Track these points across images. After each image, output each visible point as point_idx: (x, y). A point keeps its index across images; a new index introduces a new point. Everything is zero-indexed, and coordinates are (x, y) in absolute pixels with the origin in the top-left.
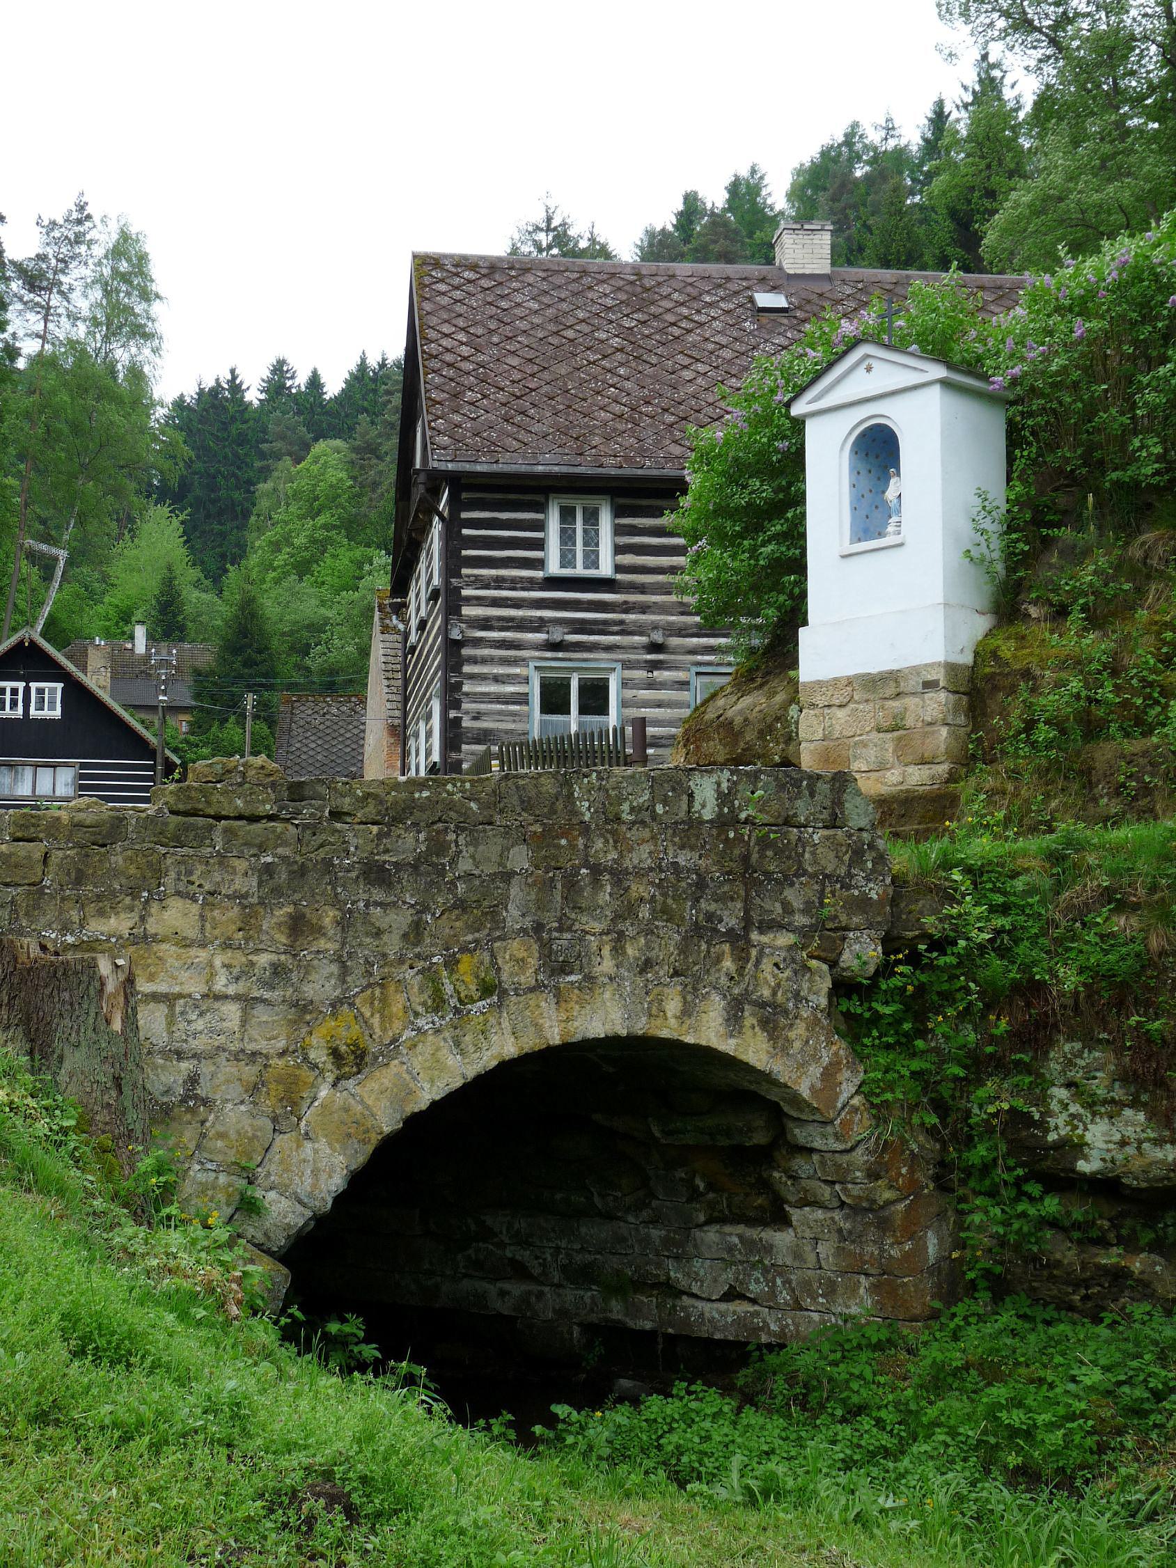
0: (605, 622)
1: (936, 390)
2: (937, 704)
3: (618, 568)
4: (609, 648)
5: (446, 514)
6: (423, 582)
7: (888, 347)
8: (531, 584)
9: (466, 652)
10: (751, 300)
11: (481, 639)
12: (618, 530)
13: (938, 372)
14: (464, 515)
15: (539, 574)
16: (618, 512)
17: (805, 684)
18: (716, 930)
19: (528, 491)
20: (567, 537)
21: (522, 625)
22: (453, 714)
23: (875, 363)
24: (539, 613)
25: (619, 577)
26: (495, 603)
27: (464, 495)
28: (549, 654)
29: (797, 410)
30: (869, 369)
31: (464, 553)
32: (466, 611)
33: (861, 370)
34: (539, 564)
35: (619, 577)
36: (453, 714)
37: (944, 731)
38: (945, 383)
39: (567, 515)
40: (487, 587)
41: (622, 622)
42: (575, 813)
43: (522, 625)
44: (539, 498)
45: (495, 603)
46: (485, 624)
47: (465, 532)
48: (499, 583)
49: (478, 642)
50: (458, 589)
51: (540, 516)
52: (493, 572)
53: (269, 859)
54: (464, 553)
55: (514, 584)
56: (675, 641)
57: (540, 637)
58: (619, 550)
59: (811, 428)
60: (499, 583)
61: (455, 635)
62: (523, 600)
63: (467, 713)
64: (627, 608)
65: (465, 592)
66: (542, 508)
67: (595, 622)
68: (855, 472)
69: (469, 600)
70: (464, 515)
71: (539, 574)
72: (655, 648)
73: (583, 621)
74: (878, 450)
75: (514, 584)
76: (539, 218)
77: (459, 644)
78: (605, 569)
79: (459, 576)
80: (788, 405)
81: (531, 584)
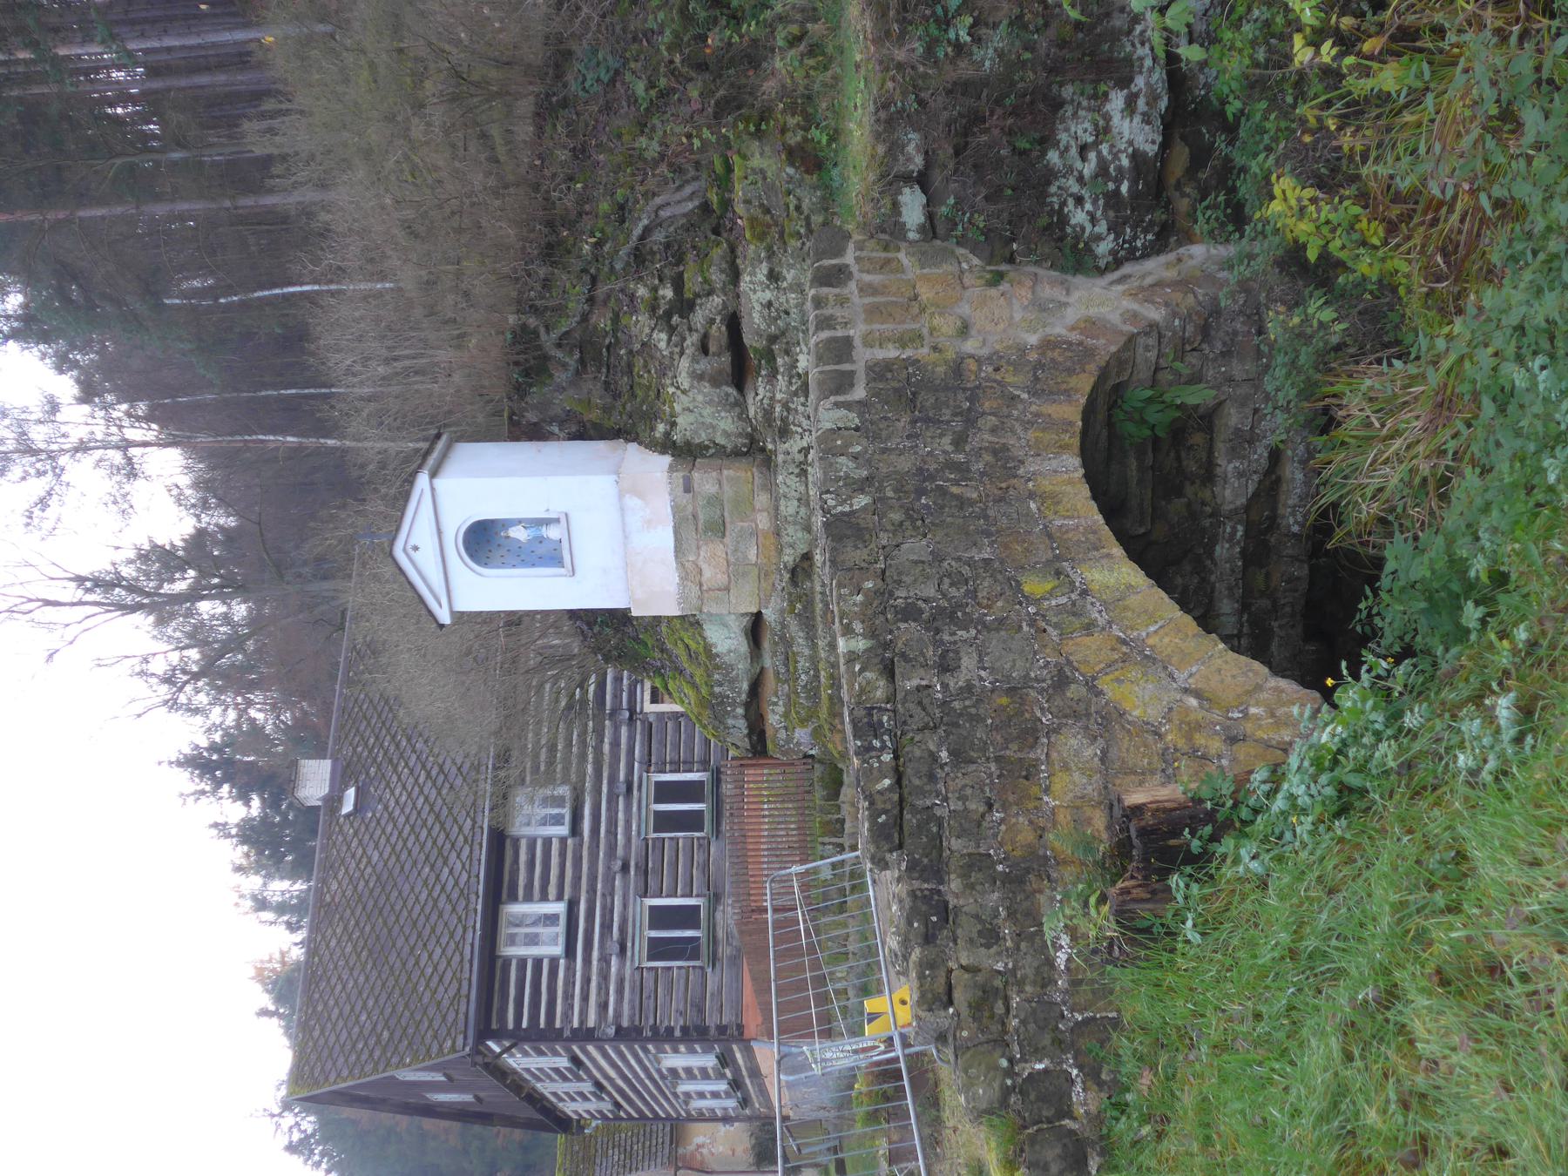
0: (603, 908)
1: (438, 482)
2: (706, 481)
3: (560, 898)
4: (625, 906)
5: (507, 1044)
6: (561, 1087)
7: (398, 529)
8: (570, 970)
9: (625, 1024)
10: (348, 816)
11: (615, 1010)
12: (529, 898)
13: (423, 480)
14: (511, 1026)
15: (562, 962)
16: (513, 898)
17: (683, 598)
18: (969, 409)
19: (491, 965)
20: (533, 940)
21: (604, 976)
22: (677, 1033)
23: (412, 542)
24: (595, 962)
25: (566, 897)
26: (585, 998)
27: (494, 1026)
28: (629, 954)
29: (445, 617)
30: (416, 548)
31: (542, 1025)
32: (591, 1023)
33: (416, 556)
34: (554, 961)
35: (566, 897)
36: (677, 1033)
37: (725, 472)
38: (434, 474)
39: (512, 940)
40: (572, 1007)
41: (603, 895)
42: (864, 509)
43: (604, 976)
44: (499, 963)
45: (585, 998)
46: (603, 1006)
47: (525, 1024)
48: (568, 996)
49: (618, 1015)
50: (574, 1031)
51: (514, 963)
52: (559, 1001)
53: (944, 754)
54: (542, 1025)
55: (569, 983)
56: (620, 852)
57: (614, 961)
58: (544, 898)
59: (461, 606)
60: (568, 996)
61: (611, 1031)
62: (583, 975)
63: (676, 1021)
64: (592, 890)
65: (576, 1024)
66: (507, 962)
67: (603, 916)
68: (503, 565)
69: (583, 1021)
70: (511, 1026)
71: (562, 962)
72: (625, 868)
73: (602, 926)
74: (483, 540)
75: (569, 983)
76: (270, 1124)
77: (619, 1029)
78: (559, 908)
79: (561, 1029)
80: (442, 626)
81: (570, 970)
